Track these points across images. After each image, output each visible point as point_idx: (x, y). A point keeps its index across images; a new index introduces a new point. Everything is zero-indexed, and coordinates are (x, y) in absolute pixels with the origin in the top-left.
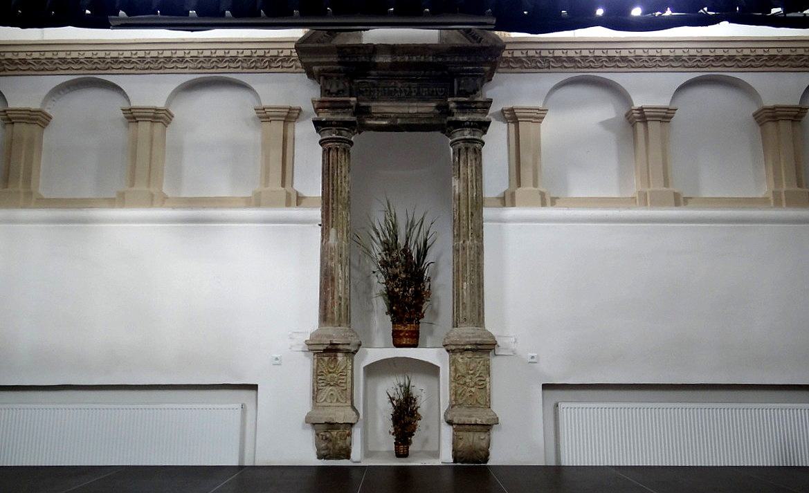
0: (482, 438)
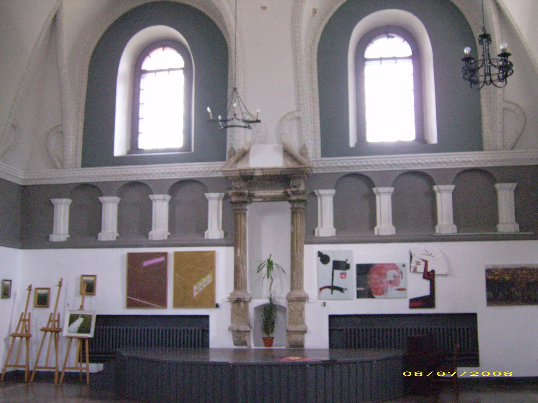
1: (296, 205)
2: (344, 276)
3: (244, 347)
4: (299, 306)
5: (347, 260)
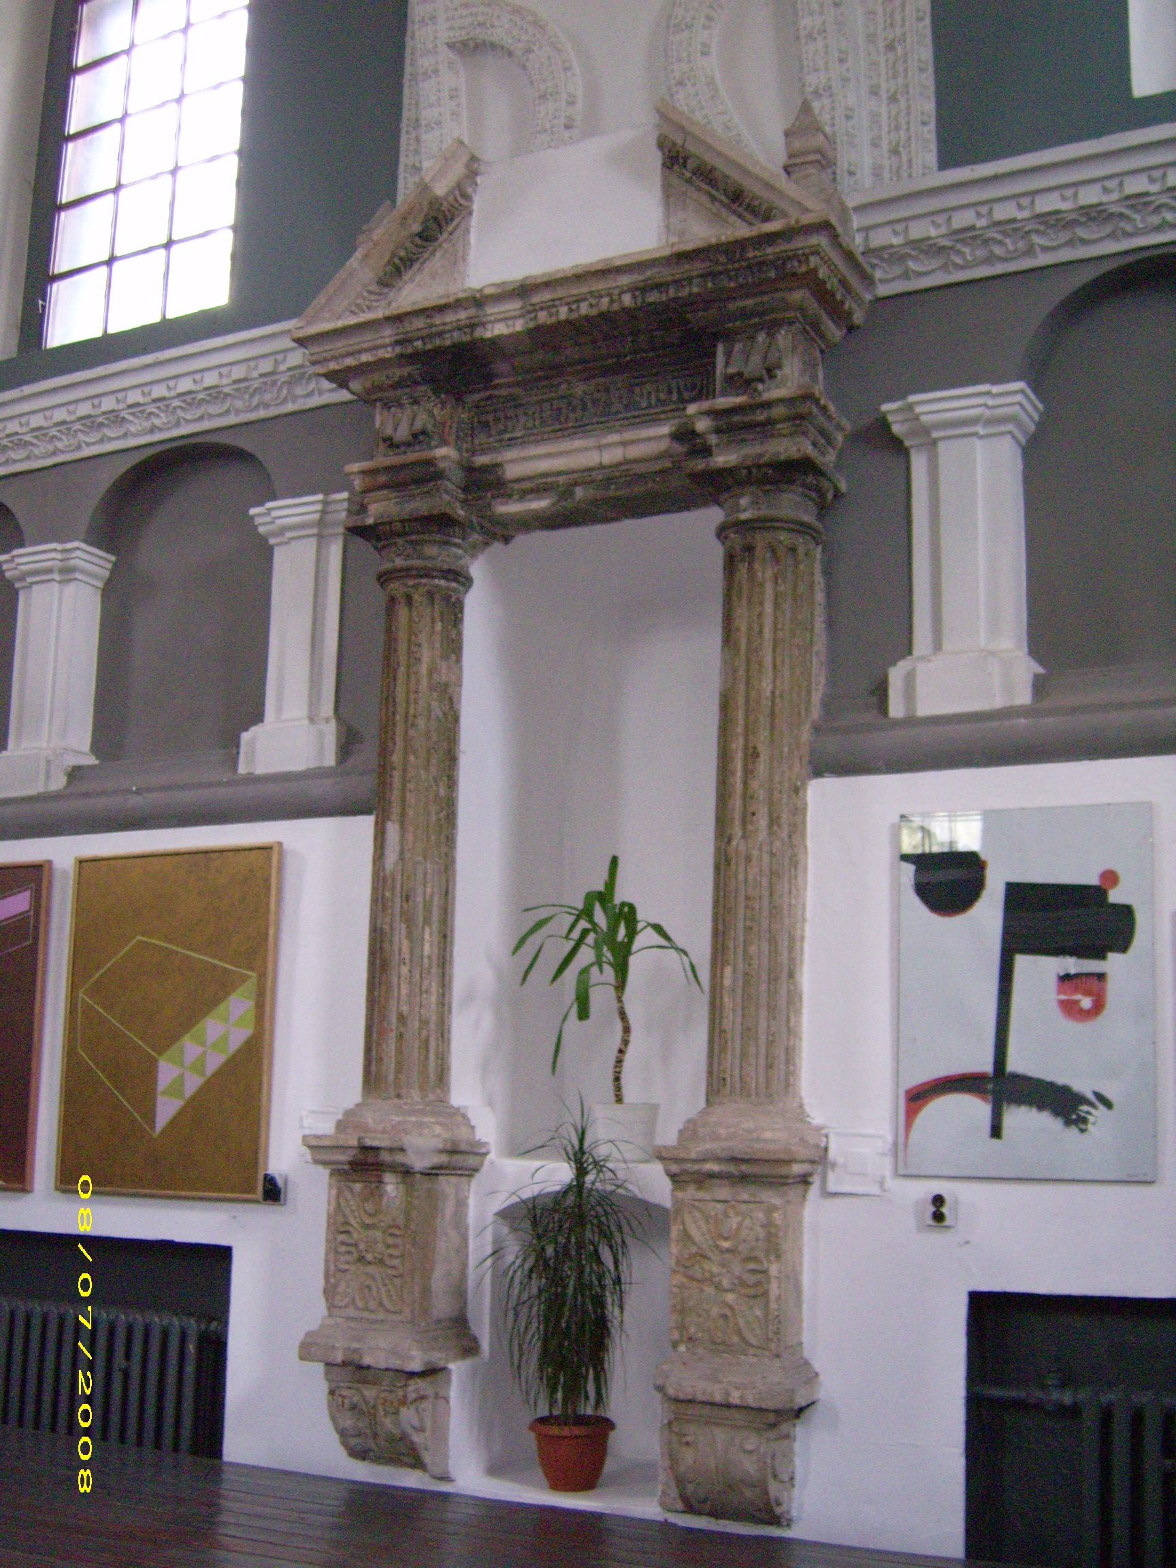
0: (749, 1447)
1: (747, 507)
2: (1086, 1003)
3: (410, 1479)
4: (745, 1215)
5: (1110, 878)
